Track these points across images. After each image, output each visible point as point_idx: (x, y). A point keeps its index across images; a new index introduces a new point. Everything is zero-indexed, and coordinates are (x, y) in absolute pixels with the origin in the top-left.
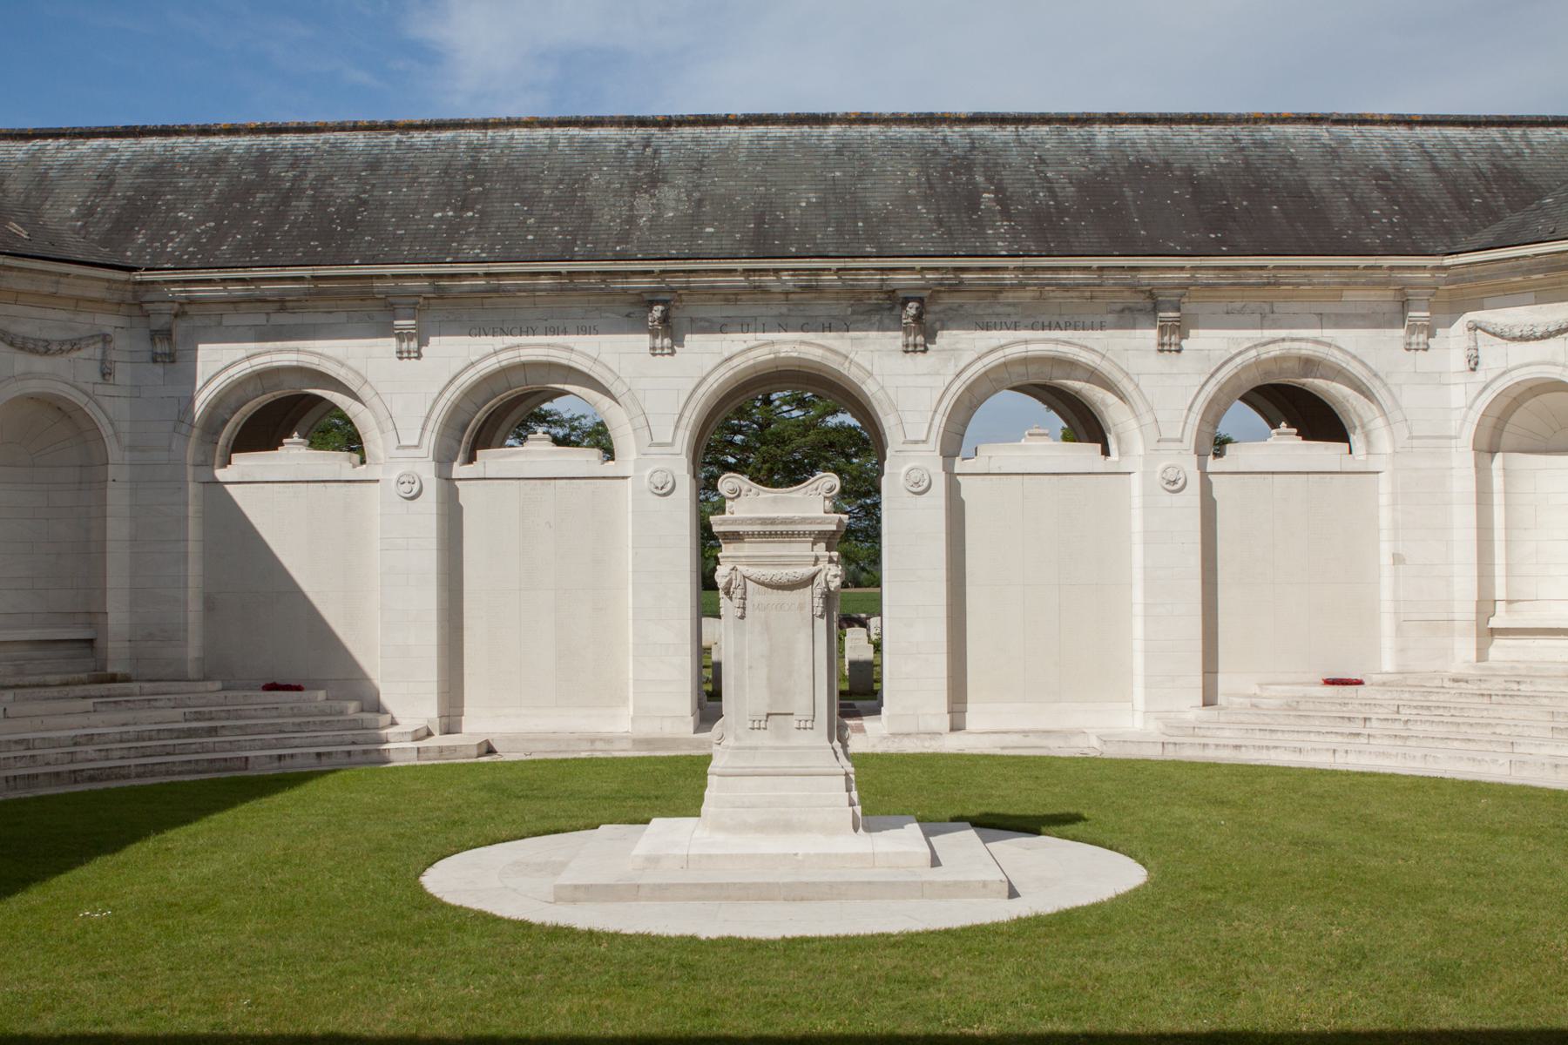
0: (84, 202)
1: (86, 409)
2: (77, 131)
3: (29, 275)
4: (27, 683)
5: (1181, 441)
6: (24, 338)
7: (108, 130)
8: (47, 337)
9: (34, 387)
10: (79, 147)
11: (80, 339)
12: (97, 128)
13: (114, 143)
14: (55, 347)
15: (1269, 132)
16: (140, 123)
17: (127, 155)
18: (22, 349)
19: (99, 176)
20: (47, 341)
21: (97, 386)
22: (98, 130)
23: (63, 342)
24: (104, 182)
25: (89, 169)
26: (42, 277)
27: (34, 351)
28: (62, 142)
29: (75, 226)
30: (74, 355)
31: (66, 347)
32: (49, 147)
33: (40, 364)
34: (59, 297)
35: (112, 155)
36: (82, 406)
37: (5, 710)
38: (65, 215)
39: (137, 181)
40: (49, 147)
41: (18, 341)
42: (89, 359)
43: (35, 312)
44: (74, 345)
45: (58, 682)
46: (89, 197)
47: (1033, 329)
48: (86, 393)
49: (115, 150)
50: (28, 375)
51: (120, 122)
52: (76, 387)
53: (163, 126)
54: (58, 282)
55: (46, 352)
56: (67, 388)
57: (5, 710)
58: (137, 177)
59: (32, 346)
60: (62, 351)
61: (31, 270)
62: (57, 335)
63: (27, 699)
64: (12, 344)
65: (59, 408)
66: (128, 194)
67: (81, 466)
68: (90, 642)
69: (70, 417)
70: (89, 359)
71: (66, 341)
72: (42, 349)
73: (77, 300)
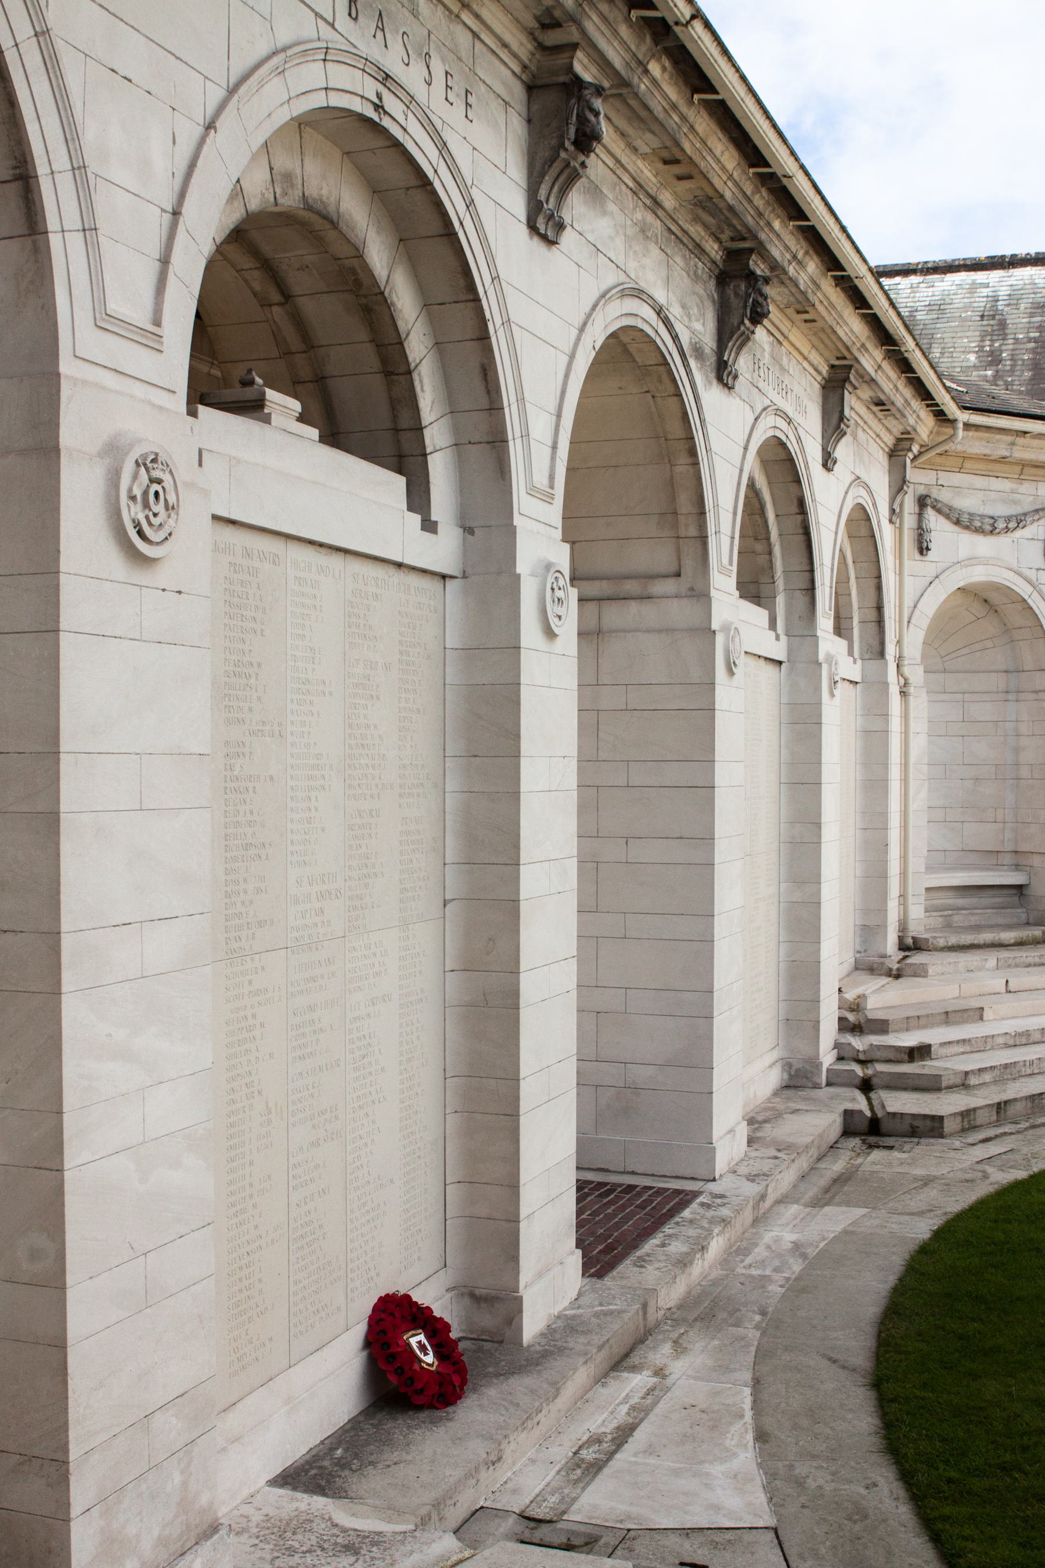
0: (981, 348)
1: (1030, 601)
2: (930, 265)
3: (987, 435)
4: (982, 942)
5: (679, 575)
6: (970, 514)
7: (969, 263)
8: (991, 513)
9: (978, 575)
11: (1025, 514)
12: (954, 261)
13: (980, 276)
14: (1001, 525)
15: (163, 240)
17: (1003, 292)
18: (967, 528)
19: (982, 316)
20: (992, 518)
23: (1008, 519)
24: (992, 322)
25: (965, 309)
26: (998, 437)
27: (979, 531)
29: (986, 376)
30: (1019, 533)
31: (1012, 525)
32: (900, 287)
33: (984, 545)
34: (1011, 463)
35: (985, 292)
36: (1026, 597)
37: (1007, 981)
38: (964, 364)
39: (1033, 320)
41: (965, 518)
42: (1032, 539)
43: (979, 482)
44: (1020, 521)
45: (1012, 941)
46: (983, 341)
48: (1029, 582)
49: (987, 286)
50: (972, 561)
51: (981, 252)
52: (1020, 574)
53: (1037, 254)
54: (1013, 444)
55: (991, 532)
56: (1011, 575)
57: (1007, 981)
58: (1032, 315)
60: (1007, 530)
61: (988, 428)
62: (1000, 510)
63: (1009, 966)
64: (958, 522)
65: (986, 601)
66: (1032, 335)
67: (1006, 672)
68: (1019, 888)
69: (996, 611)
70: (1032, 539)
71: (1012, 516)
72: (988, 528)
73: (1023, 465)
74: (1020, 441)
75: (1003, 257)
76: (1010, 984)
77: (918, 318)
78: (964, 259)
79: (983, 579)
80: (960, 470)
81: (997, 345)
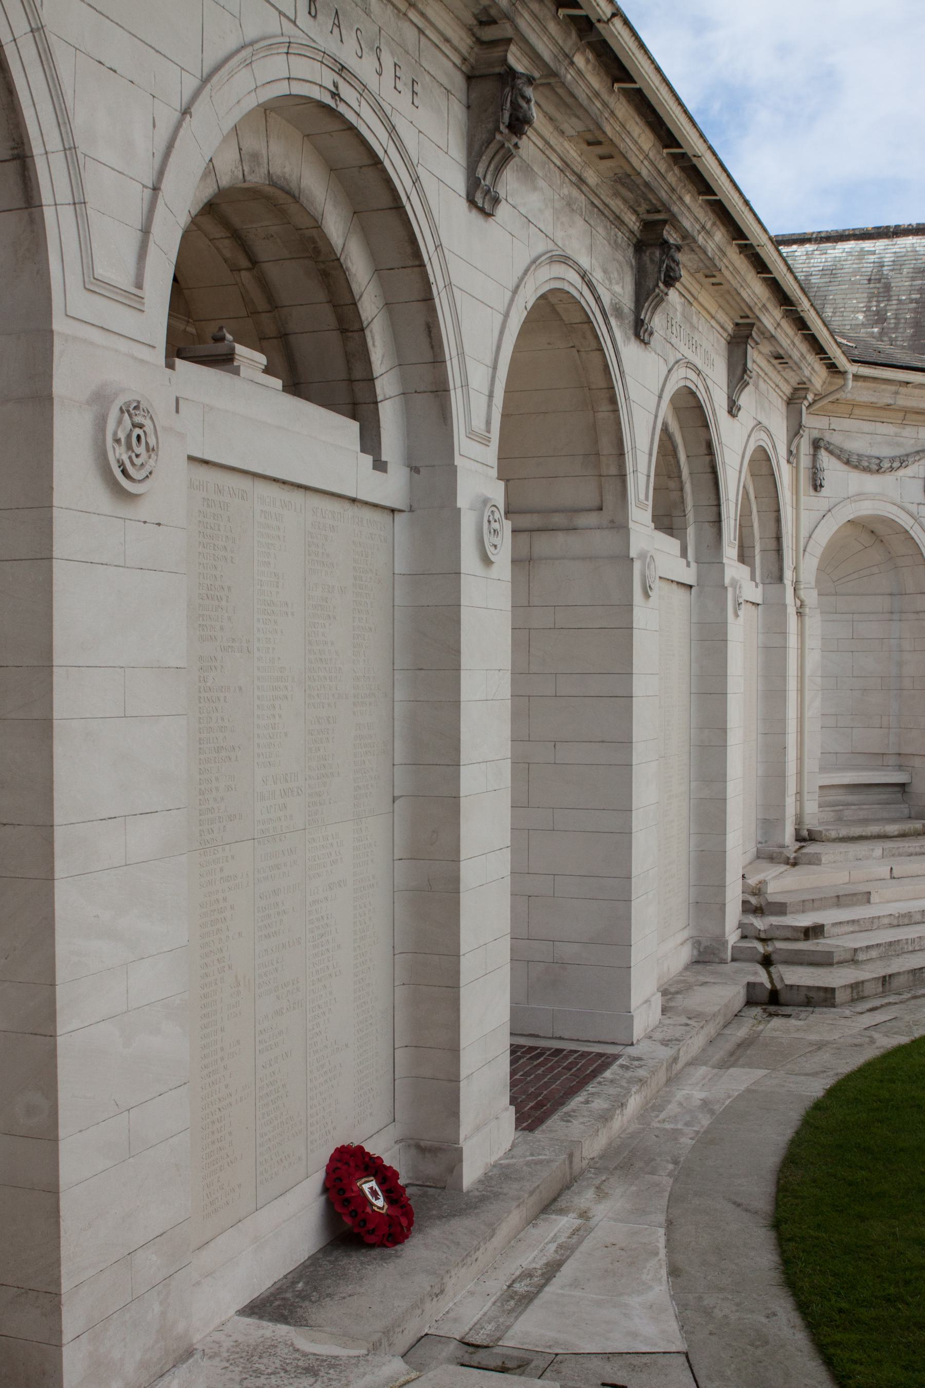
0: (868, 308)
1: (911, 532)
2: (823, 235)
3: (873, 385)
4: (869, 834)
6: (858, 455)
8: (877, 454)
9: (866, 509)
10: (829, 251)
11: (907, 455)
12: (844, 231)
13: (867, 245)
14: (886, 465)
16: (892, 223)
17: (888, 258)
18: (856, 467)
19: (869, 280)
20: (878, 458)
21: (921, 506)
22: (847, 233)
23: (892, 459)
24: (878, 285)
25: (854, 273)
26: (884, 387)
28: (809, 247)
29: (873, 333)
30: (901, 472)
31: (896, 465)
32: (796, 254)
33: (871, 483)
35: (872, 258)
36: (908, 529)
37: (891, 869)
39: (915, 283)
40: (796, 254)
41: (854, 459)
43: (867, 426)
45: (896, 833)
46: (870, 302)
47: (625, 475)
48: (911, 515)
49: (874, 253)
50: (860, 496)
52: (903, 509)
53: (918, 224)
54: (897, 393)
56: (894, 509)
57: (891, 869)
58: (913, 279)
59: (866, 464)
60: (892, 469)
61: (875, 379)
62: (886, 451)
63: (893, 855)
64: (848, 463)
65: (872, 532)
66: (914, 296)
68: (903, 786)
69: (882, 541)
70: (914, 477)
71: (896, 457)
72: (875, 467)
73: (906, 412)
74: (903, 390)
75: (888, 227)
76: (894, 871)
77: (813, 281)
78: (853, 230)
79: (870, 512)
80: (850, 416)
81: (882, 305)
